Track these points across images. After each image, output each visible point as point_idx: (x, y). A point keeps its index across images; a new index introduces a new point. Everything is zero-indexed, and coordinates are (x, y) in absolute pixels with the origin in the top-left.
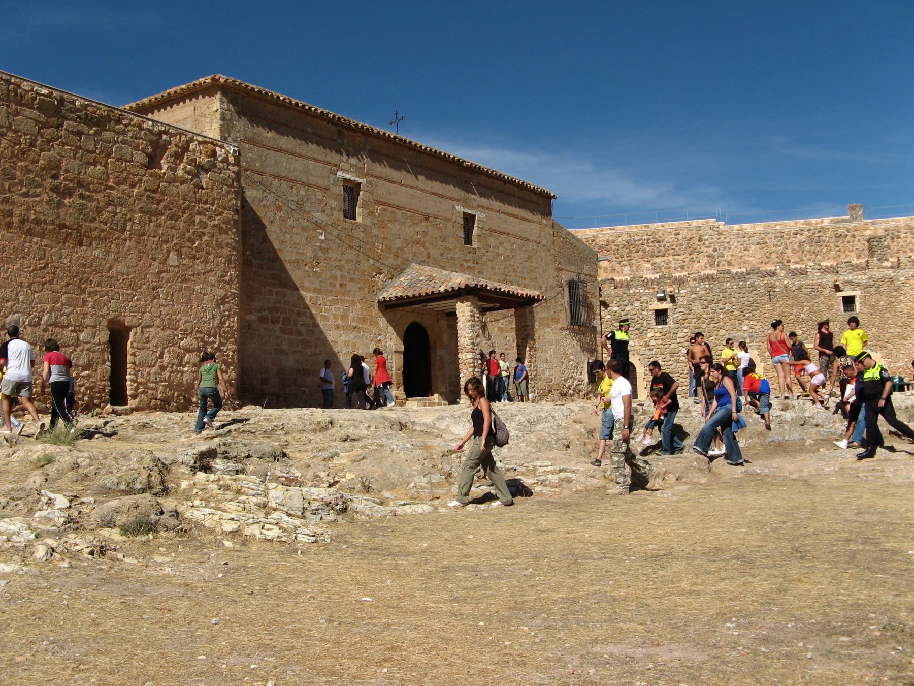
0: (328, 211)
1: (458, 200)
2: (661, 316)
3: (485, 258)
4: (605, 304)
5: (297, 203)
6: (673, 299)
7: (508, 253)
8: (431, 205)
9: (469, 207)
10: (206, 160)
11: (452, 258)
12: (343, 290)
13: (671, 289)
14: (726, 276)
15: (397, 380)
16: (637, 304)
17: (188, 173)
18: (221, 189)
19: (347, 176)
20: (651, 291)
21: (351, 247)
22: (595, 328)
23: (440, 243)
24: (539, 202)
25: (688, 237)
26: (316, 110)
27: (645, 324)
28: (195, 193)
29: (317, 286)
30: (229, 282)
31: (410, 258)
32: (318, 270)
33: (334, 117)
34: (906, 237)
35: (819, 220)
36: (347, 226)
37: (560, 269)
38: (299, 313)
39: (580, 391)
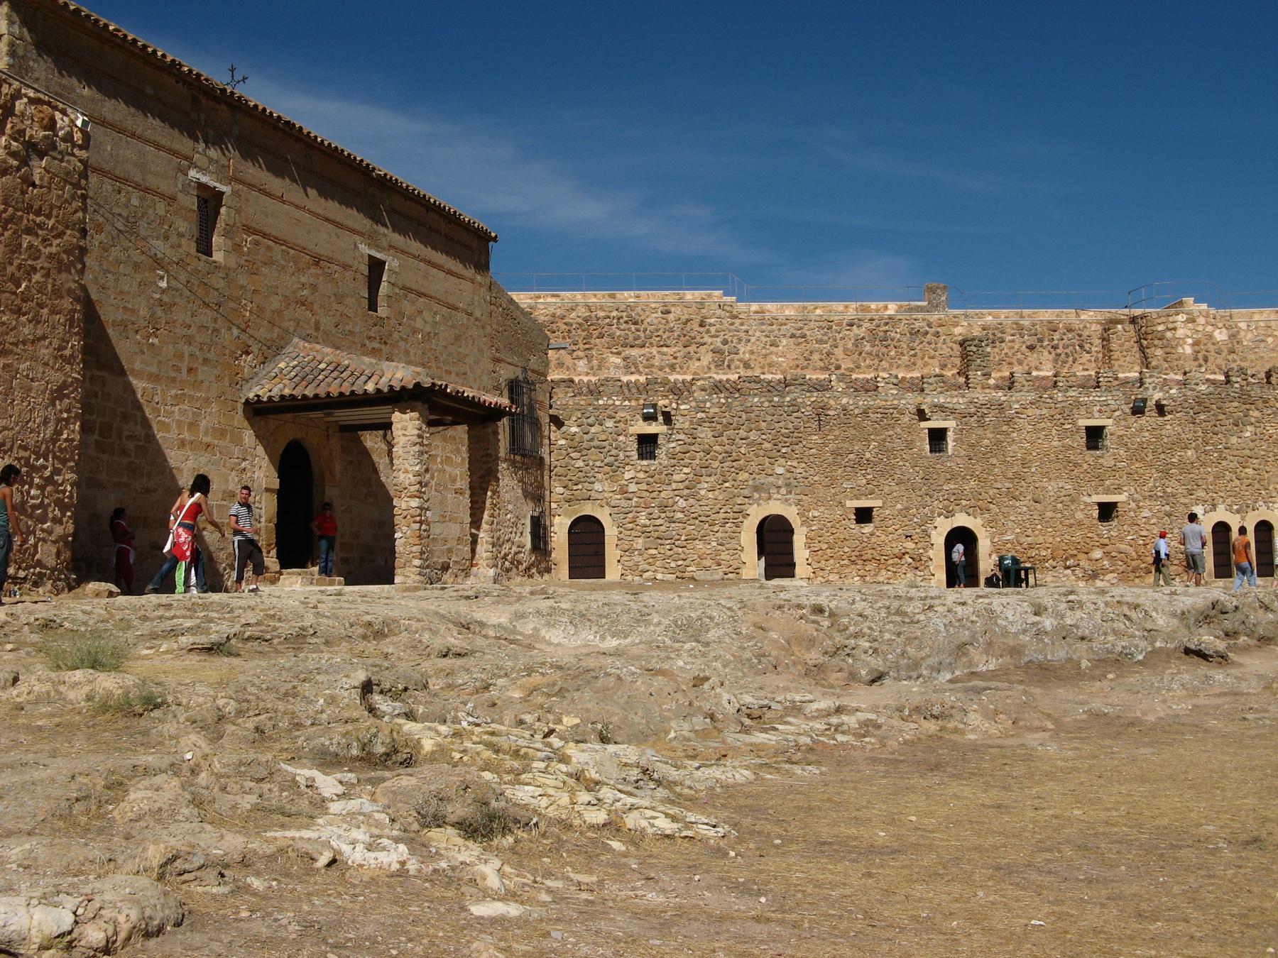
0: (173, 239)
1: (362, 234)
2: (647, 444)
3: (396, 336)
4: (557, 422)
5: (127, 219)
6: (668, 418)
7: (428, 328)
8: (325, 240)
9: (379, 248)
10: (42, 133)
11: (351, 333)
12: (191, 379)
13: (666, 402)
14: (753, 385)
15: (268, 539)
16: (610, 423)
17: (13, 155)
18: (63, 189)
19: (204, 179)
20: (633, 403)
21: (207, 305)
22: (542, 459)
23: (335, 306)
24: (466, 243)
25: (683, 318)
26: (164, 56)
27: (621, 456)
28: (24, 192)
29: (154, 369)
30: (69, 360)
31: (291, 329)
32: (156, 341)
33: (190, 71)
34: (1013, 341)
35: (881, 304)
36: (201, 266)
37: (497, 360)
38: (125, 417)
39: (520, 563)
